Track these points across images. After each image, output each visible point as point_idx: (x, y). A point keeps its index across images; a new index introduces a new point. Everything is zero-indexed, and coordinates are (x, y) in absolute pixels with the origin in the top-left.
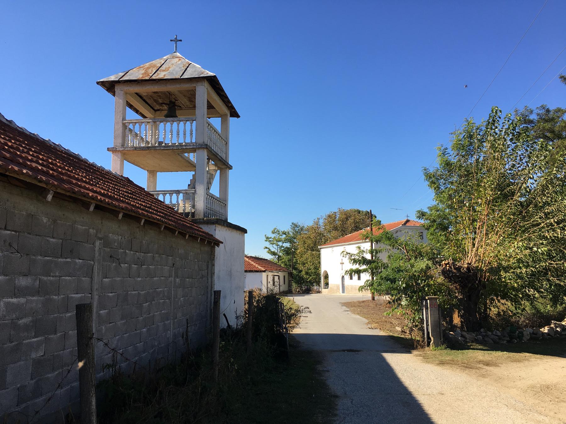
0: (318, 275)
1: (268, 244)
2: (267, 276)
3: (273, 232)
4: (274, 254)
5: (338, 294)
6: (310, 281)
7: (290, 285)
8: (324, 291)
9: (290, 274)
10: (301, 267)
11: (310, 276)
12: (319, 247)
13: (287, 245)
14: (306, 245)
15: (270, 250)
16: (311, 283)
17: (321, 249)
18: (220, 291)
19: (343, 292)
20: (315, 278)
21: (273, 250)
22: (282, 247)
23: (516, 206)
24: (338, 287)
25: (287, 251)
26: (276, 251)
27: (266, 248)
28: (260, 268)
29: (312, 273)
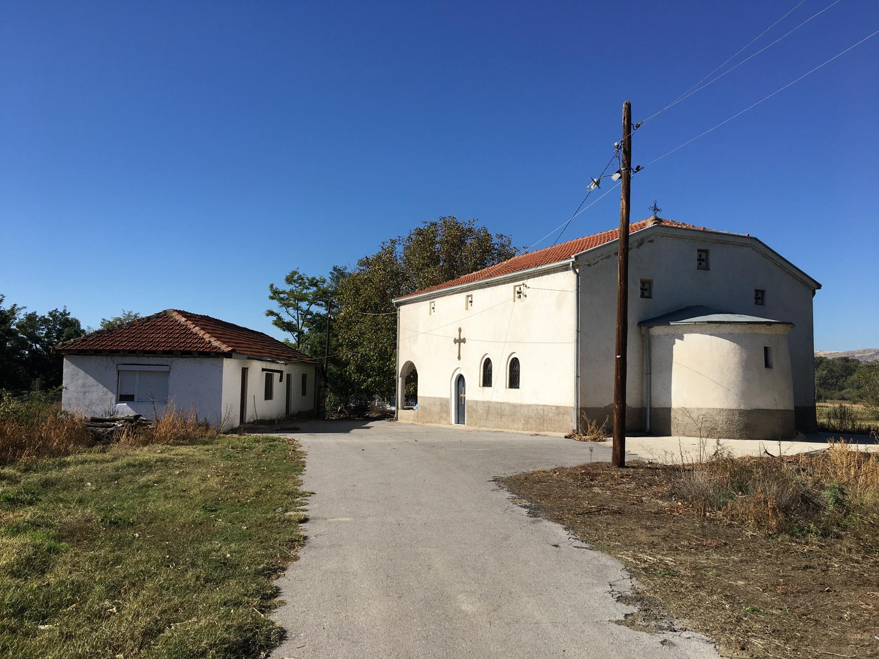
0: (391, 373)
1: (275, 306)
2: (245, 372)
3: (289, 280)
4: (288, 327)
5: (443, 425)
6: (366, 390)
7: (319, 399)
8: (403, 415)
9: (321, 372)
10: (345, 354)
11: (369, 376)
12: (394, 301)
13: (319, 310)
14: (361, 300)
15: (279, 318)
16: (369, 394)
17: (399, 304)
18: (490, 386)
19: (460, 418)
20: (379, 384)
21: (287, 318)
22: (308, 312)
23: (228, 457)
24: (444, 403)
25: (319, 323)
26: (295, 322)
27: (271, 313)
28: (216, 343)
29: (373, 369)
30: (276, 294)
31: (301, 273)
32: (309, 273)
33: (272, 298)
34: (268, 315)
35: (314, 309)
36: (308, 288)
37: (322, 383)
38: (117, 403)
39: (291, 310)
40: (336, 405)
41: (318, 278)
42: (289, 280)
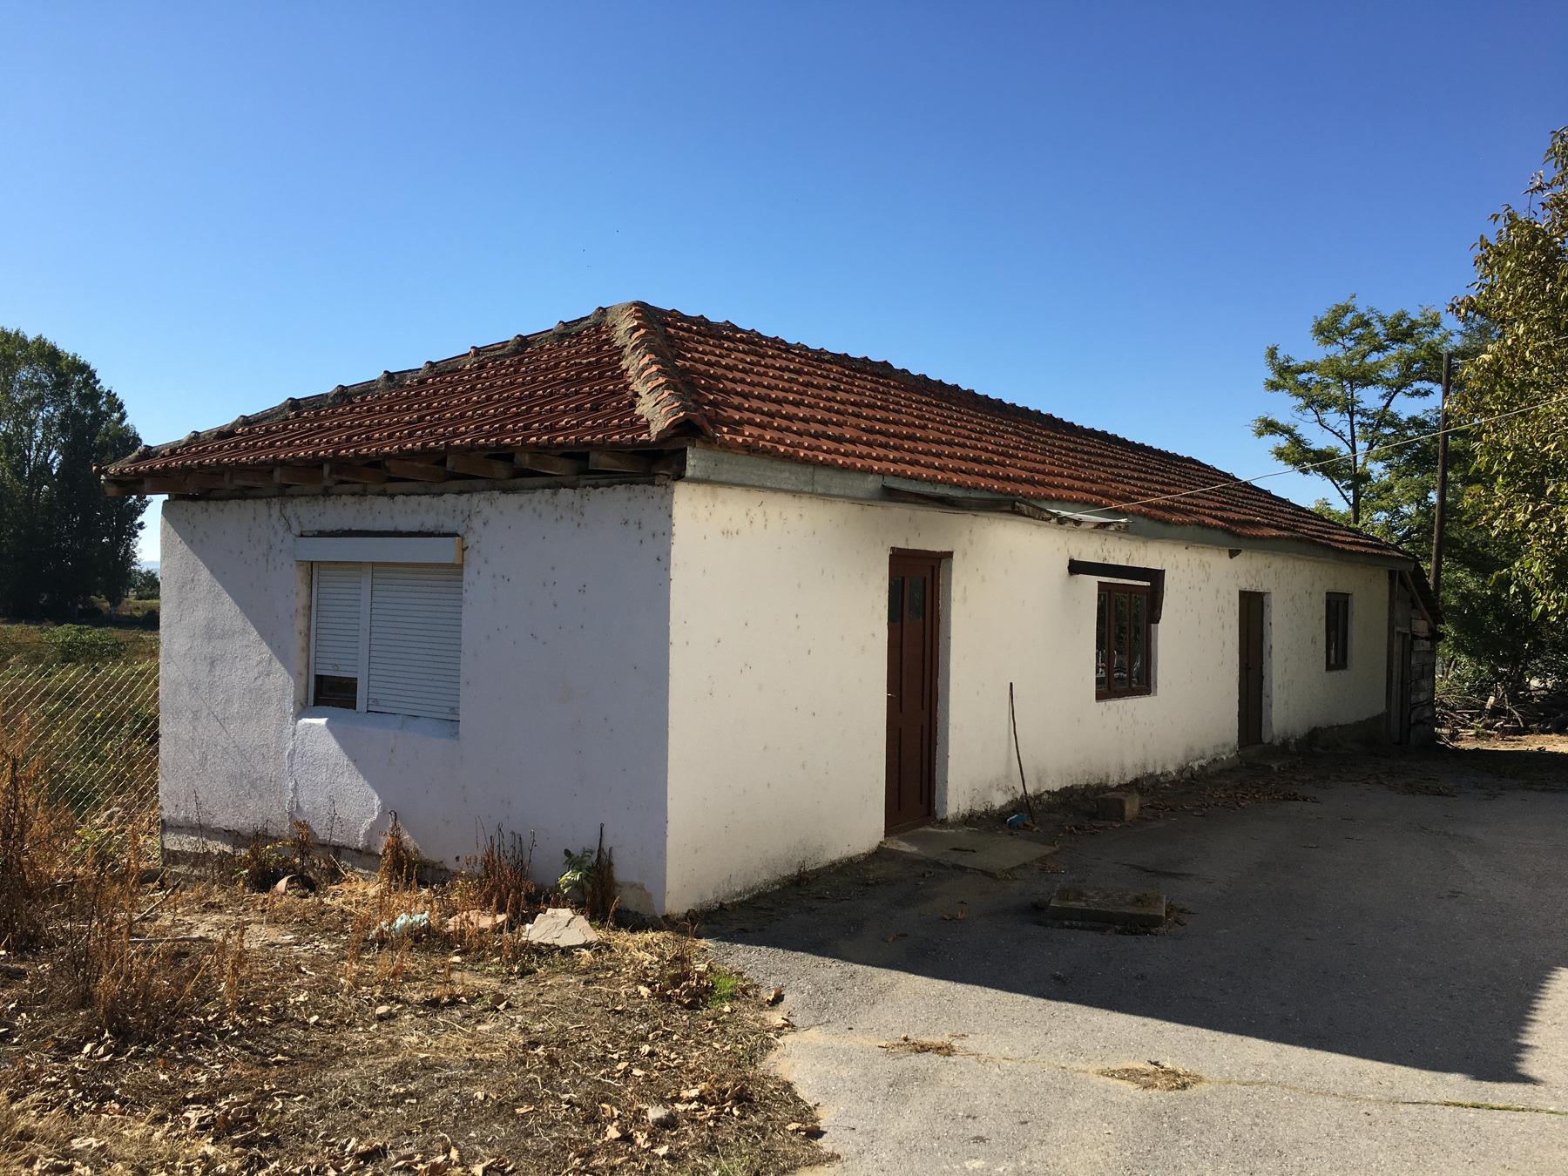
1: (1284, 407)
9: (1411, 590)
13: (1422, 404)
15: (1297, 441)
21: (1319, 440)
22: (1384, 418)
25: (1430, 453)
27: (1270, 427)
30: (1284, 375)
31: (1362, 310)
32: (1384, 300)
33: (1274, 386)
34: (1260, 434)
35: (1405, 407)
36: (1379, 348)
37: (1421, 627)
38: (299, 715)
39: (1333, 417)
40: (1484, 691)
41: (1415, 316)
42: (1327, 331)
